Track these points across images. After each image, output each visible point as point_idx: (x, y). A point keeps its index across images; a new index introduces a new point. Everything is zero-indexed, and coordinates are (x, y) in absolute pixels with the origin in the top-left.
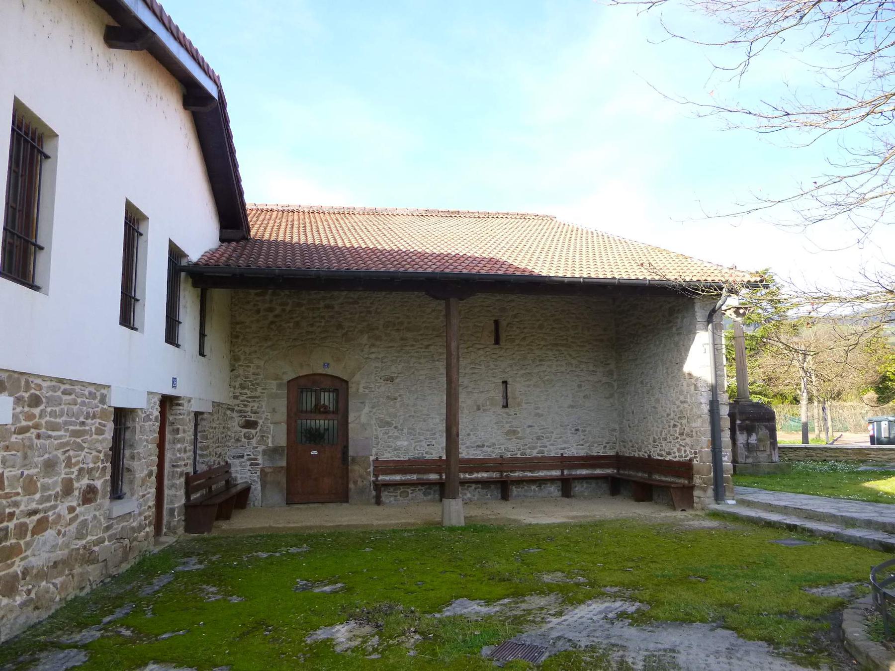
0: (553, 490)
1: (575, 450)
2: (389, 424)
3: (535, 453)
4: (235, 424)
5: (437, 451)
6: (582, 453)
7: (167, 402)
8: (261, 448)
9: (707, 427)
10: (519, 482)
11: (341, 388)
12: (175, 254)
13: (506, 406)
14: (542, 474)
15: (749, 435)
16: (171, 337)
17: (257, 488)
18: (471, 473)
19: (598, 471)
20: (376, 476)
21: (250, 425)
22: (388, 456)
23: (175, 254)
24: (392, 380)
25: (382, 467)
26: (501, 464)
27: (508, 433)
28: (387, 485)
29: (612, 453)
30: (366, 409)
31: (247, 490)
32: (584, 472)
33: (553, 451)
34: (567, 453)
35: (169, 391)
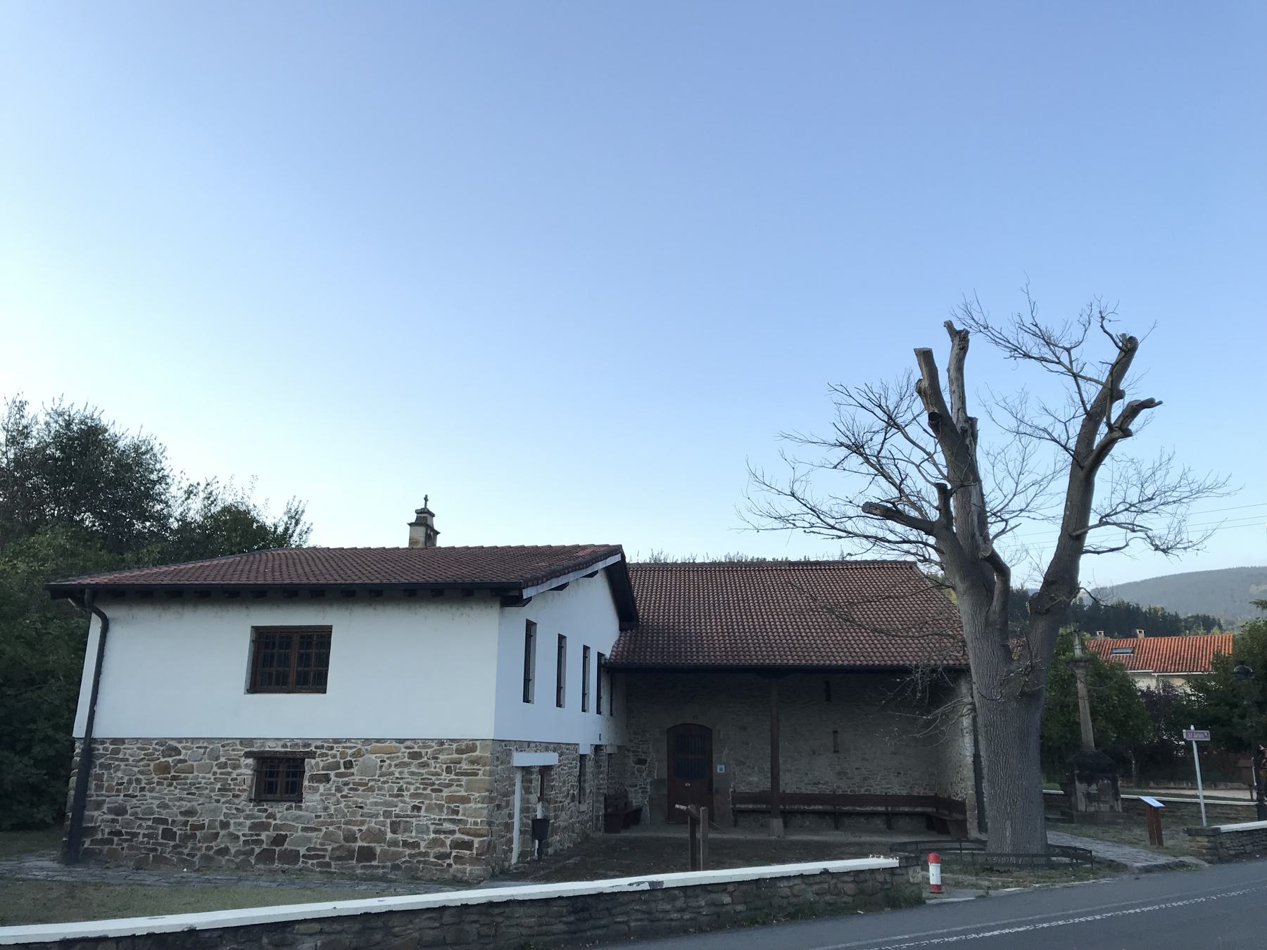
0: (879, 822)
1: (896, 789)
2: (744, 763)
3: (862, 791)
4: (631, 761)
5: (766, 785)
6: (904, 793)
7: (597, 748)
8: (648, 780)
9: (971, 774)
10: (849, 814)
11: (706, 734)
12: (600, 655)
13: (836, 752)
14: (869, 809)
15: (1089, 785)
16: (599, 712)
17: (647, 811)
18: (809, 805)
19: (919, 809)
20: (734, 804)
21: (641, 762)
22: (743, 788)
23: (600, 655)
24: (745, 729)
25: (739, 798)
26: (834, 798)
27: (839, 773)
28: (742, 812)
29: (932, 794)
30: (726, 751)
31: (639, 811)
32: (907, 809)
33: (878, 790)
34: (891, 792)
35: (598, 743)
